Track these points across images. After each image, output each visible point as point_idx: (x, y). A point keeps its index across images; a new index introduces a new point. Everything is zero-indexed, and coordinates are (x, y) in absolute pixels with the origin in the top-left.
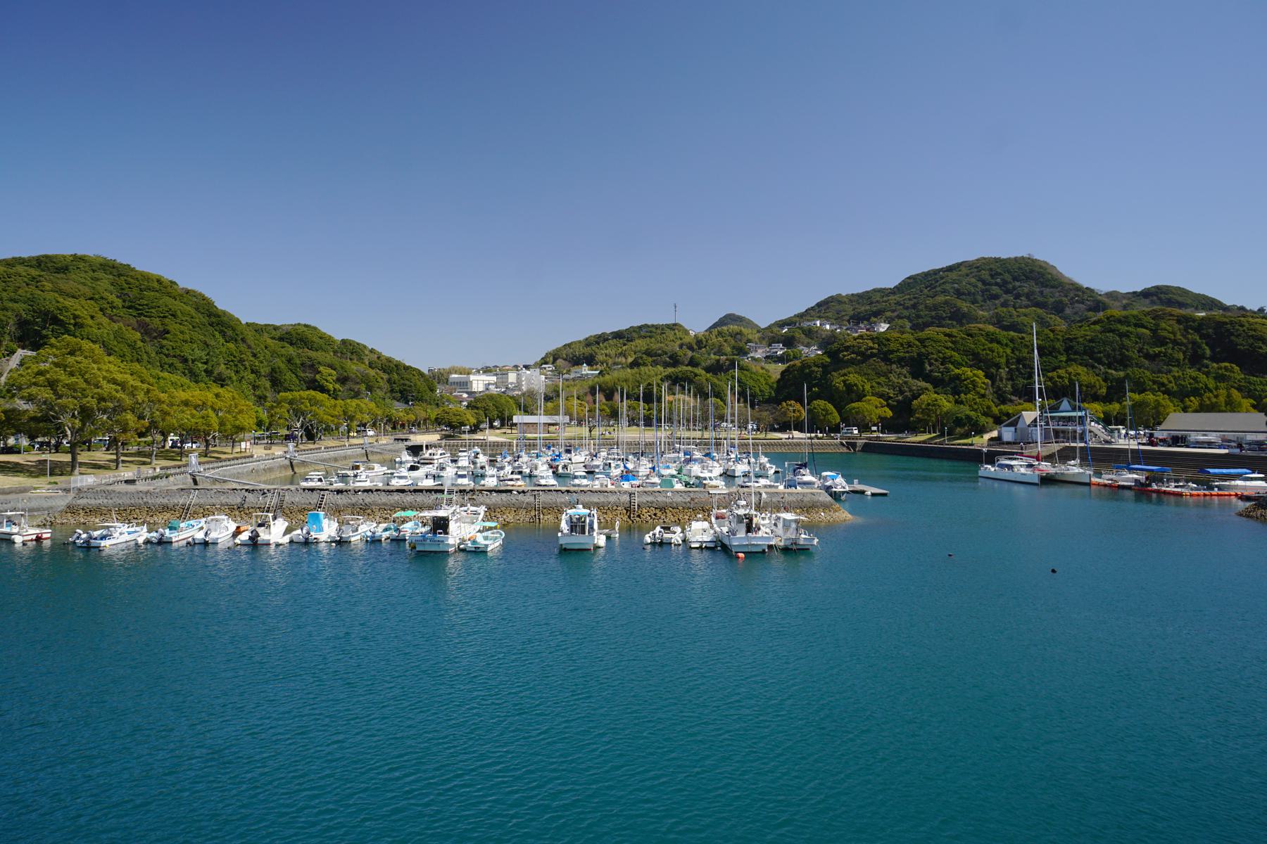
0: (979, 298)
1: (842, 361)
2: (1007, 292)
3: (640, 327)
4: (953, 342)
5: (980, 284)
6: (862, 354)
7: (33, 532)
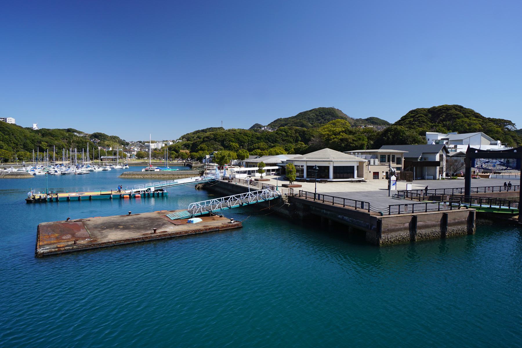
0: (314, 120)
2: (323, 118)
3: (210, 128)
7: (40, 195)
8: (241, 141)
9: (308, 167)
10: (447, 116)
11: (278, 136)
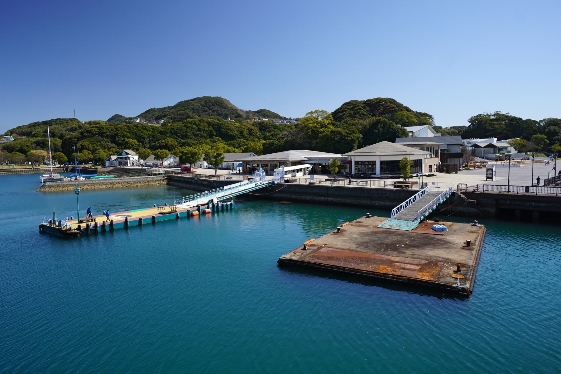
0: (200, 111)
1: (84, 136)
2: (210, 109)
3: (57, 120)
4: (129, 129)
5: (201, 106)
6: (93, 134)
8: (139, 137)
9: (382, 162)
10: (385, 109)
11: (188, 130)
